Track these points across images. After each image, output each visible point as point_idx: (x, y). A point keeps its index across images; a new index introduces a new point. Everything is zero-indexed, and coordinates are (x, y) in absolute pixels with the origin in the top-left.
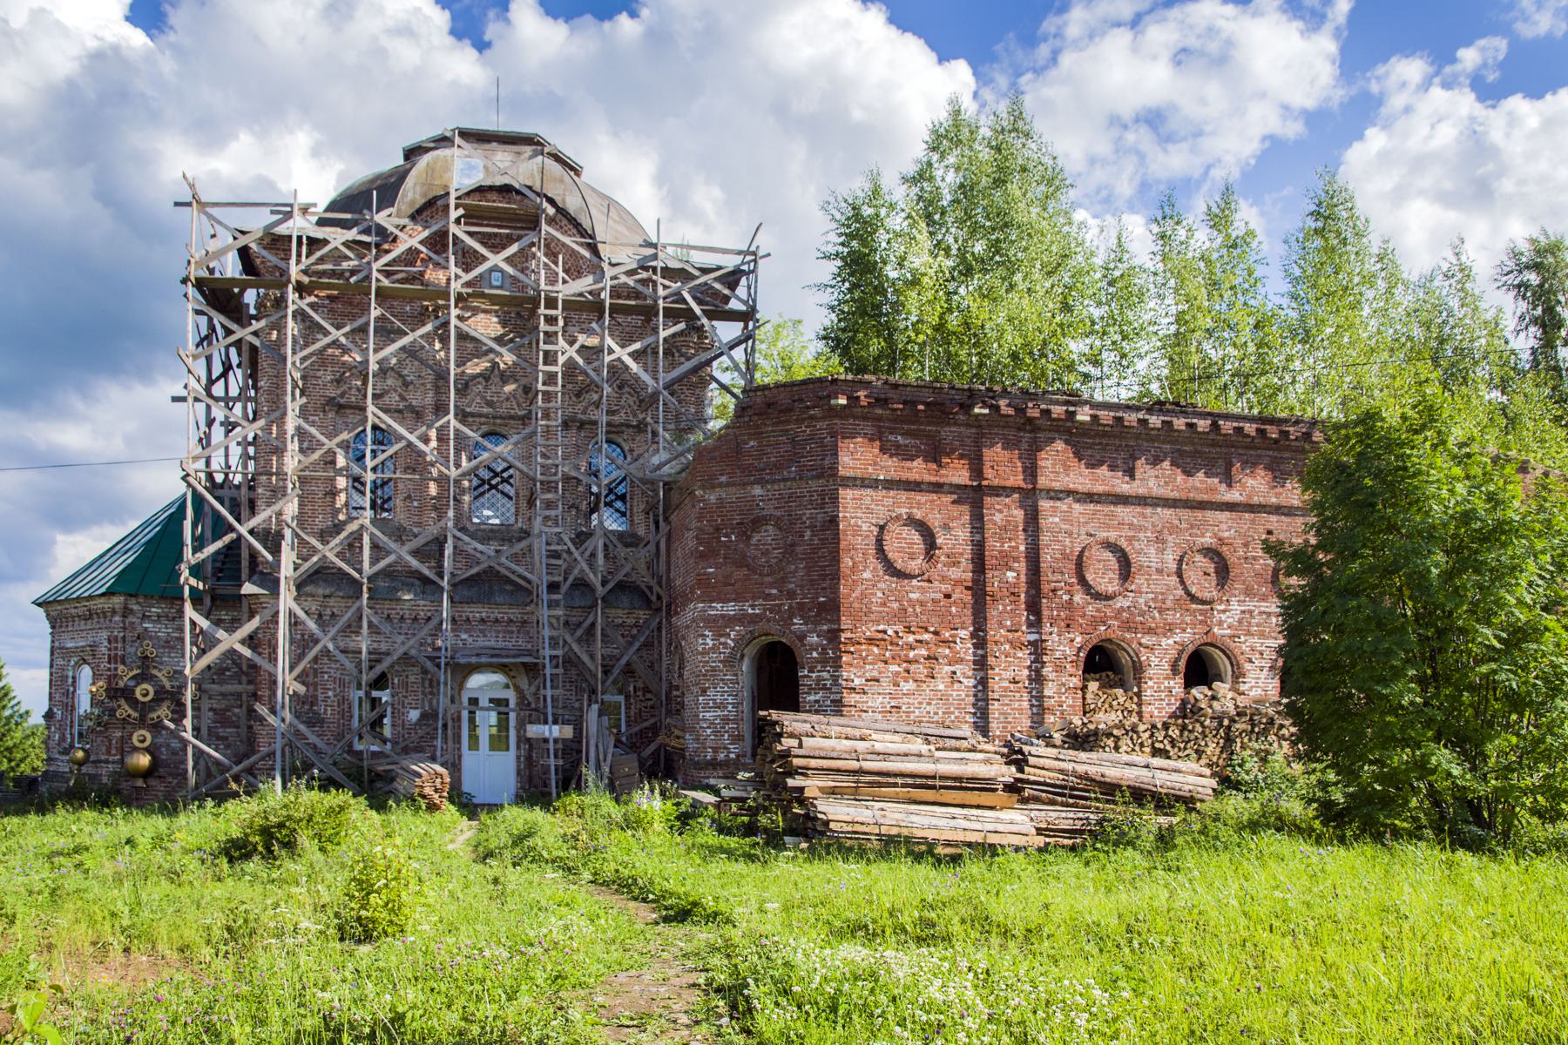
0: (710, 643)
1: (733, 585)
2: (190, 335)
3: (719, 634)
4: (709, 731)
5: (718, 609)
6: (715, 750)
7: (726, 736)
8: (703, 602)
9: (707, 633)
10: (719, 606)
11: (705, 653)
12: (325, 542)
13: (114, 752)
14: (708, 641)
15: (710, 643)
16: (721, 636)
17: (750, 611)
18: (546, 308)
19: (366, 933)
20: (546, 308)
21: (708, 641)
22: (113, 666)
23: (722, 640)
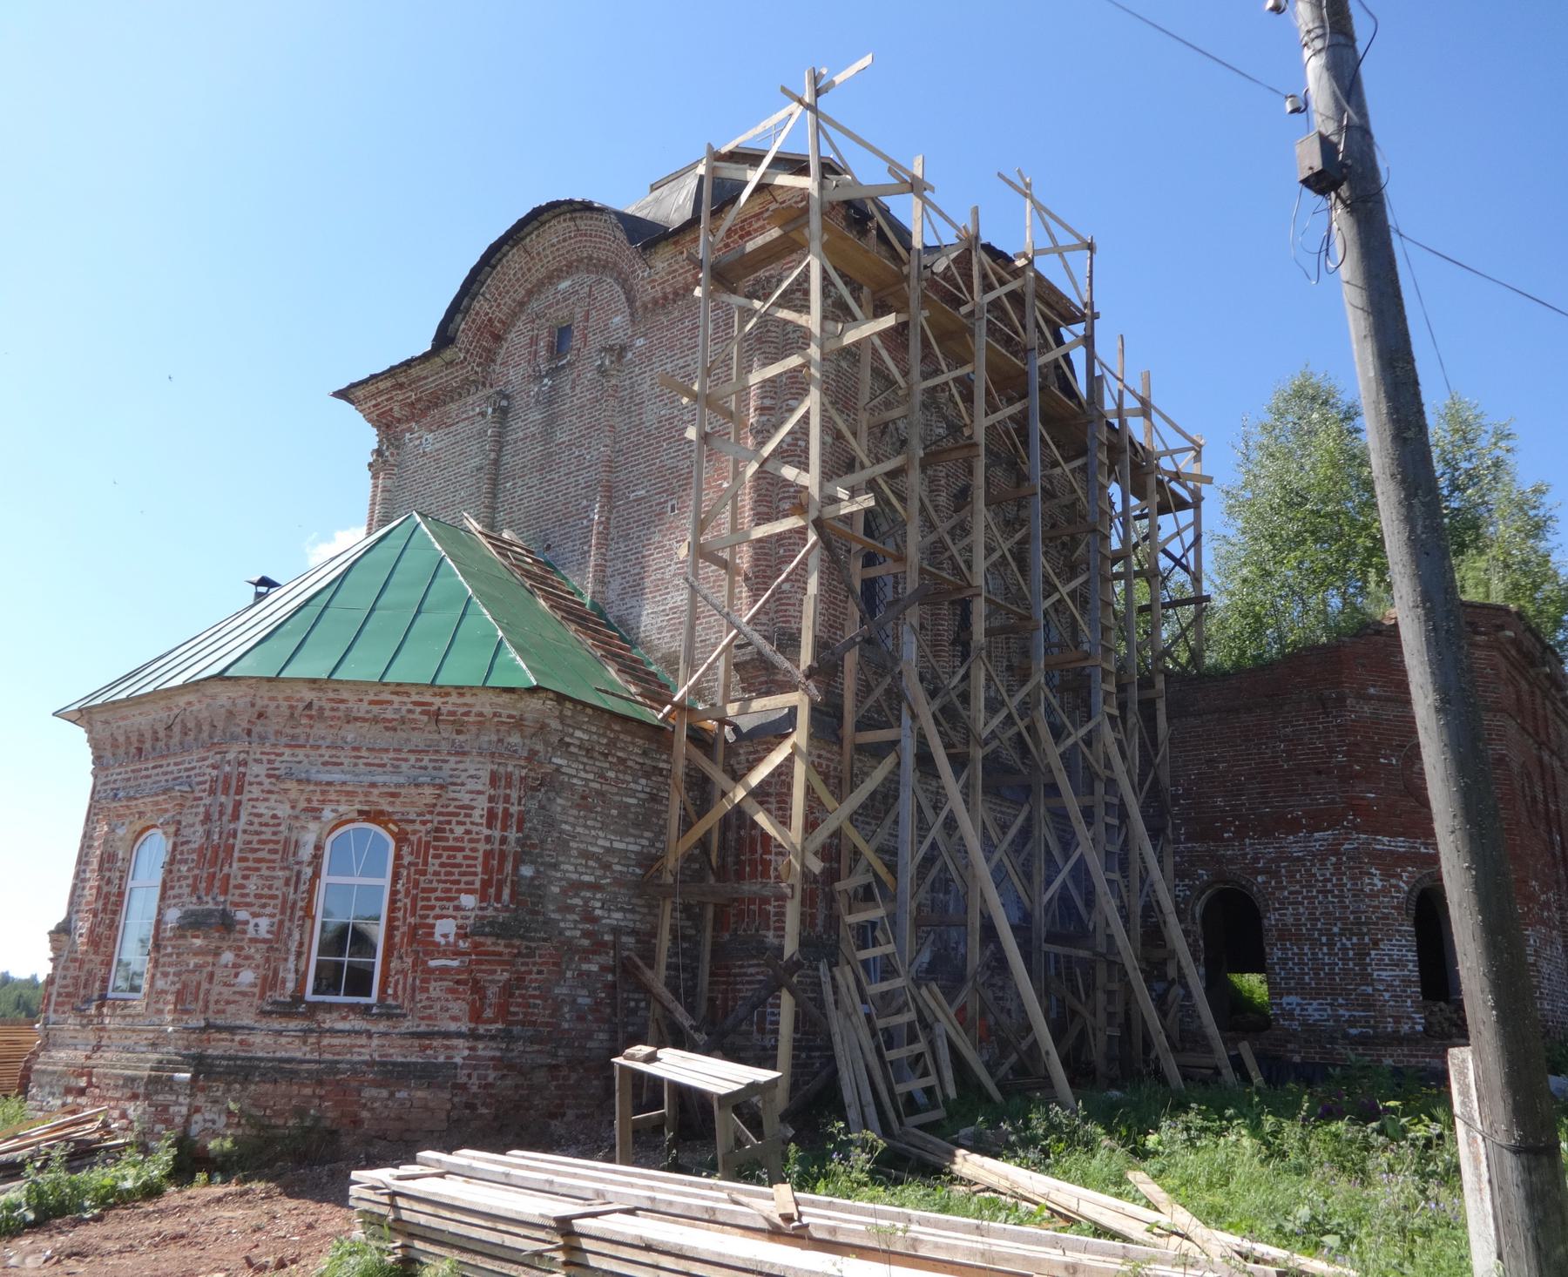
0: (1380, 884)
1: (1400, 816)
2: (759, 129)
3: (1387, 875)
4: (1387, 995)
5: (1384, 843)
6: (1397, 1020)
7: (1409, 1003)
8: (1365, 832)
9: (1373, 871)
10: (1386, 839)
11: (1372, 895)
12: (1056, 589)
13: (489, 1013)
14: (1376, 881)
15: (1380, 884)
16: (1393, 876)
17: (1423, 850)
18: (369, 994)
19: (264, 581)
20: (369, 994)
21: (1376, 881)
22: (501, 792)
23: (1393, 881)
